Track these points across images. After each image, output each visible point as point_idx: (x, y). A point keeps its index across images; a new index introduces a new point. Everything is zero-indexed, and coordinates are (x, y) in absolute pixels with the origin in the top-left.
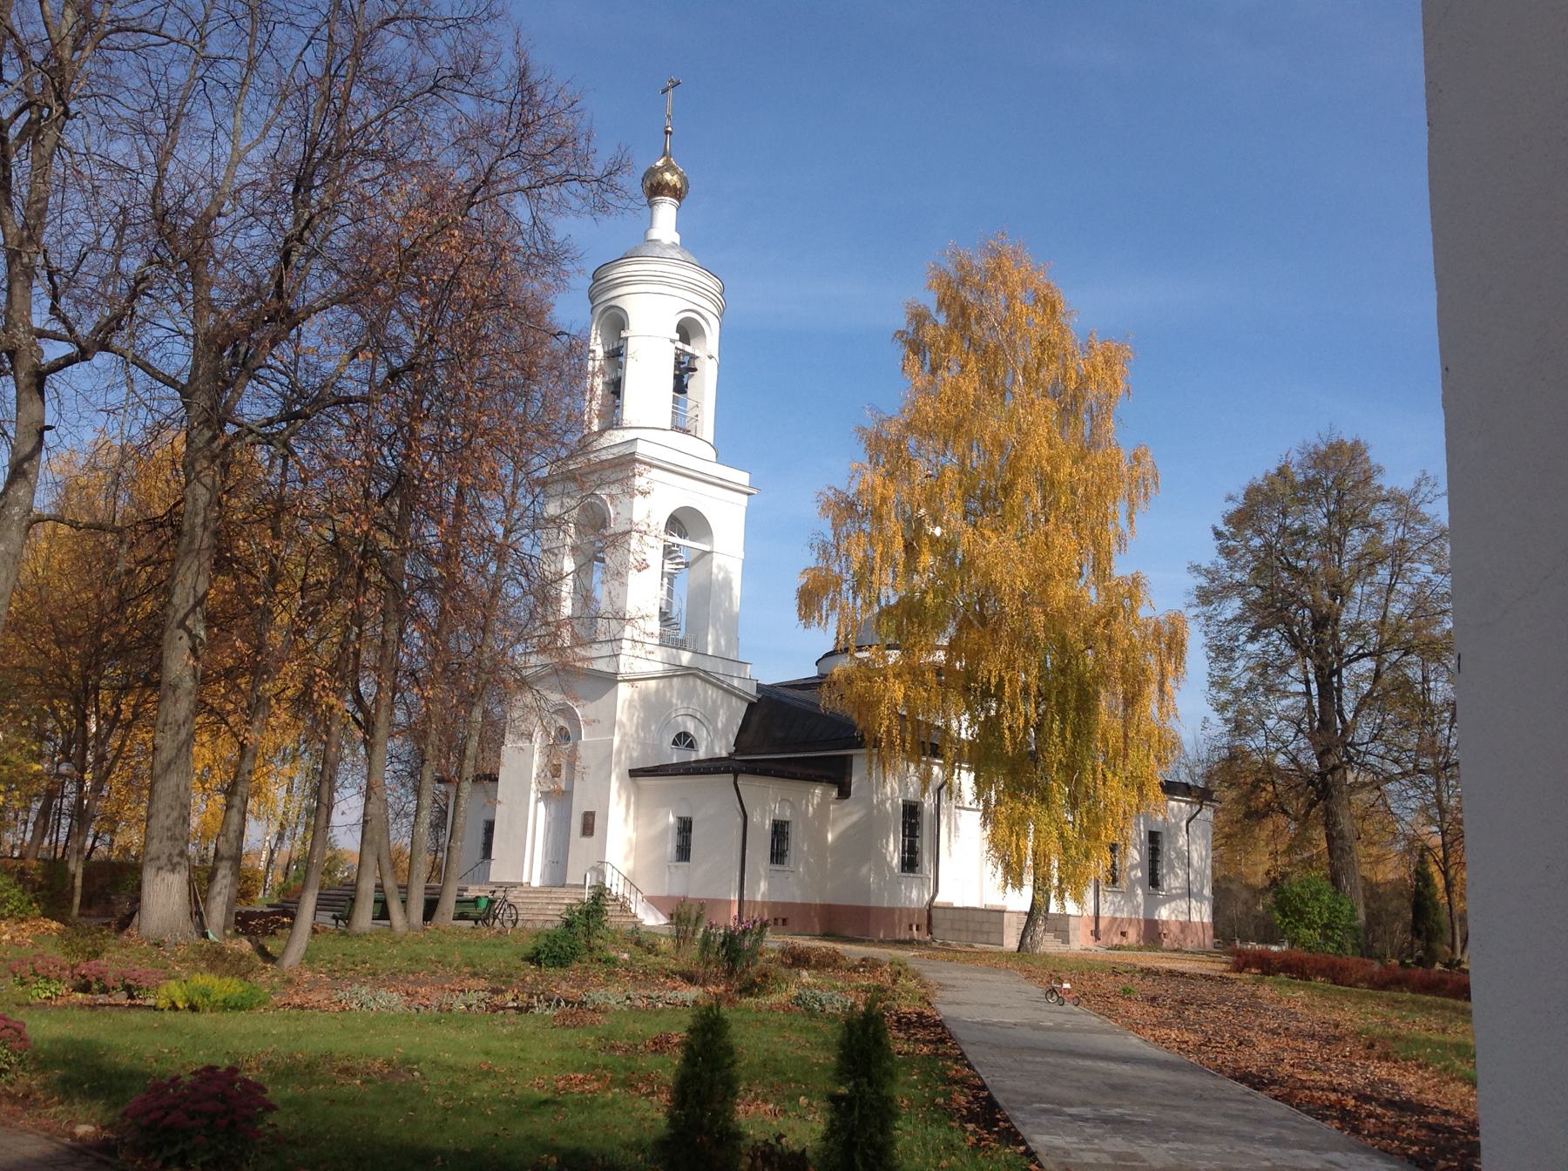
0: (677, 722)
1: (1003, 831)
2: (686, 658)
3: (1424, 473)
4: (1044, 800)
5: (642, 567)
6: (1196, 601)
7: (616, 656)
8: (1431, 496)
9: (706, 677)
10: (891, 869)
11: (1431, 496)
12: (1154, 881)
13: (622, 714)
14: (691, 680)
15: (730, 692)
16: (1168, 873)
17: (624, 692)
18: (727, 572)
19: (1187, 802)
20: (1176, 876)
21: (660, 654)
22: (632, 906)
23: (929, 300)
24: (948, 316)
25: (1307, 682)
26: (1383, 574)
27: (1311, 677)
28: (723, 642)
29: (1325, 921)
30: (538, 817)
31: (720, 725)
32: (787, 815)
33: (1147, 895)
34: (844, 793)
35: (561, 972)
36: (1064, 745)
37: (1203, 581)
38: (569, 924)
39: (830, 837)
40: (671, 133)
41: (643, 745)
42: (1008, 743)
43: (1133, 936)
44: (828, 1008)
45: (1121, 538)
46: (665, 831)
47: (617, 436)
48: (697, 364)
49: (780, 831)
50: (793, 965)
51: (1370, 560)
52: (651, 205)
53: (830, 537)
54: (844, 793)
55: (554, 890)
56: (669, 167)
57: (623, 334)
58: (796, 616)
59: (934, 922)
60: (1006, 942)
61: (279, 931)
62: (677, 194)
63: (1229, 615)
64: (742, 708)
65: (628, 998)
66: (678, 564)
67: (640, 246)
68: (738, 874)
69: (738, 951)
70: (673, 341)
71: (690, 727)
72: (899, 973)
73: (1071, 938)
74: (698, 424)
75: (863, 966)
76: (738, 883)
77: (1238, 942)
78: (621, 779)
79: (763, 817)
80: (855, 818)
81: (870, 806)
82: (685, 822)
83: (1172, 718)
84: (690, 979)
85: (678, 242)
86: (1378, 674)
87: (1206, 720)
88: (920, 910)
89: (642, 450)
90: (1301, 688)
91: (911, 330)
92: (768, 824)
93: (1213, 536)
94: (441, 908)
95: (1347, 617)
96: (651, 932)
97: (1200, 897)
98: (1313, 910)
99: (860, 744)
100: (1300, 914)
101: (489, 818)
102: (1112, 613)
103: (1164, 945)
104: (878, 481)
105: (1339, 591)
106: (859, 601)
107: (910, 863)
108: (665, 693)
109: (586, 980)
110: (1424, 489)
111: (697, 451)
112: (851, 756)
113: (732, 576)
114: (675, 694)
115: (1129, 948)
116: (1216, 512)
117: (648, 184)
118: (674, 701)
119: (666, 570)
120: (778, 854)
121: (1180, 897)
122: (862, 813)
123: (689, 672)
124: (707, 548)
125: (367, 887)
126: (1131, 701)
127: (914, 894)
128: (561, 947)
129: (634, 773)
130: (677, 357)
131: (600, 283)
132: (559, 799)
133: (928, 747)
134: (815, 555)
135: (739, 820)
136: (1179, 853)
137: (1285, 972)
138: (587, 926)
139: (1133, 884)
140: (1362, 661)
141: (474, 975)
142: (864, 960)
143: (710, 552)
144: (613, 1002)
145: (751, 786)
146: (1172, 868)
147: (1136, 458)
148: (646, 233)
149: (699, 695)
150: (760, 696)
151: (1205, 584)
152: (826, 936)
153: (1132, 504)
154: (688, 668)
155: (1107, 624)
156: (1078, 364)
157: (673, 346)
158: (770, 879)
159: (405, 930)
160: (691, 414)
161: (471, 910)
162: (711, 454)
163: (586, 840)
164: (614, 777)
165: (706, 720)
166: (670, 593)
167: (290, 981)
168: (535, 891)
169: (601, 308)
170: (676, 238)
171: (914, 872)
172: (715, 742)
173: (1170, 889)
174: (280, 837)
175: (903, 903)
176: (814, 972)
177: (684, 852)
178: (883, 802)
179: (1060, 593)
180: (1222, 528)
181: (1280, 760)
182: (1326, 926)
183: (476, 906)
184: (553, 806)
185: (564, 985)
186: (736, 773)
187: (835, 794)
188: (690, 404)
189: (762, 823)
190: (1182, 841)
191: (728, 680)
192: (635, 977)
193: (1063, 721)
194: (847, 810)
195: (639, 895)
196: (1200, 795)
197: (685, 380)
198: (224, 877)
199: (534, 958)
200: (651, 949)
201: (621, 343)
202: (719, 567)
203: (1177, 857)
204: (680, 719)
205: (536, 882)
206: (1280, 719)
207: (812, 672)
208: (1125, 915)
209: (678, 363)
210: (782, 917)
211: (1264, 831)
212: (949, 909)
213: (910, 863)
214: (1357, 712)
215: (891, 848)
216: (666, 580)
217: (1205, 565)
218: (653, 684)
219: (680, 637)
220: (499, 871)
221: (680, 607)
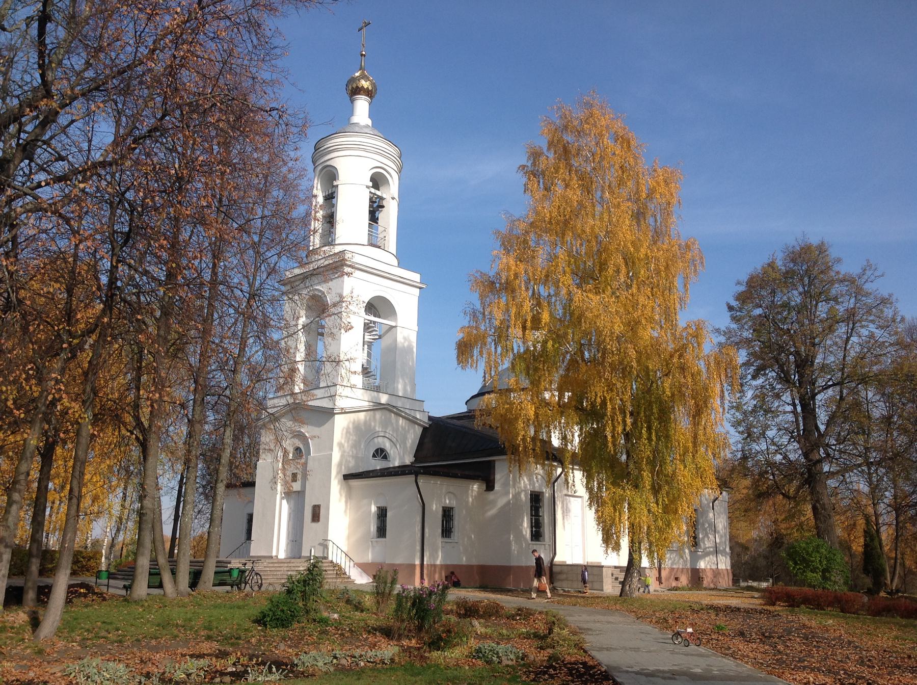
1: (608, 510)
2: (384, 399)
3: (868, 261)
4: (636, 486)
5: (349, 328)
8: (873, 277)
10: (524, 537)
11: (873, 277)
12: (695, 542)
15: (413, 421)
17: (341, 423)
22: (347, 570)
24: (555, 153)
25: (794, 405)
26: (842, 329)
27: (797, 402)
29: (824, 566)
30: (283, 509)
32: (454, 504)
34: (490, 487)
35: (282, 632)
37: (722, 339)
38: (289, 592)
40: (364, 55)
41: (356, 457)
42: (610, 445)
43: (684, 580)
44: (505, 662)
48: (384, 203)
49: (447, 514)
50: (465, 616)
52: (352, 101)
53: (478, 306)
55: (293, 560)
56: (363, 77)
57: (335, 183)
58: (456, 362)
60: (605, 588)
61: (74, 600)
62: (369, 93)
64: (419, 430)
65: (335, 657)
67: (344, 124)
69: (426, 611)
70: (368, 187)
71: (387, 446)
72: (554, 623)
74: (386, 242)
75: (520, 615)
82: (382, 510)
84: (388, 633)
85: (370, 125)
91: (529, 164)
96: (360, 591)
97: (723, 553)
99: (501, 452)
101: (250, 512)
102: (684, 348)
104: (512, 262)
106: (499, 349)
107: (537, 535)
108: (370, 425)
109: (302, 639)
110: (868, 273)
111: (386, 259)
112: (494, 461)
114: (378, 425)
115: (683, 589)
116: (729, 293)
117: (350, 87)
119: (366, 340)
120: (447, 532)
124: (393, 324)
125: (144, 563)
126: (697, 413)
128: (282, 611)
129: (347, 477)
130: (371, 199)
131: (319, 150)
132: (296, 497)
134: (468, 318)
137: (805, 604)
138: (304, 592)
141: (209, 638)
142: (519, 610)
143: (396, 327)
144: (320, 664)
145: (428, 484)
146: (706, 535)
148: (349, 119)
150: (430, 423)
152: (484, 587)
153: (686, 278)
156: (647, 182)
157: (368, 191)
159: (175, 595)
160: (381, 236)
161: (226, 577)
162: (395, 262)
163: (314, 525)
166: (369, 355)
167: (40, 652)
168: (281, 562)
169: (320, 167)
170: (369, 122)
172: (401, 456)
174: (118, 530)
176: (482, 621)
177: (382, 531)
180: (734, 303)
182: (824, 571)
183: (231, 576)
184: (292, 502)
185: (282, 646)
186: (417, 474)
187: (484, 487)
188: (380, 229)
189: (435, 508)
191: (412, 413)
193: (649, 429)
195: (352, 562)
197: (376, 215)
199: (261, 621)
200: (359, 607)
201: (334, 189)
205: (282, 555)
206: (779, 430)
207: (464, 409)
209: (372, 201)
210: (454, 578)
211: (768, 505)
212: (563, 565)
213: (537, 535)
214: (828, 424)
216: (366, 346)
218: (362, 416)
219: (376, 384)
220: (256, 550)
221: (375, 366)
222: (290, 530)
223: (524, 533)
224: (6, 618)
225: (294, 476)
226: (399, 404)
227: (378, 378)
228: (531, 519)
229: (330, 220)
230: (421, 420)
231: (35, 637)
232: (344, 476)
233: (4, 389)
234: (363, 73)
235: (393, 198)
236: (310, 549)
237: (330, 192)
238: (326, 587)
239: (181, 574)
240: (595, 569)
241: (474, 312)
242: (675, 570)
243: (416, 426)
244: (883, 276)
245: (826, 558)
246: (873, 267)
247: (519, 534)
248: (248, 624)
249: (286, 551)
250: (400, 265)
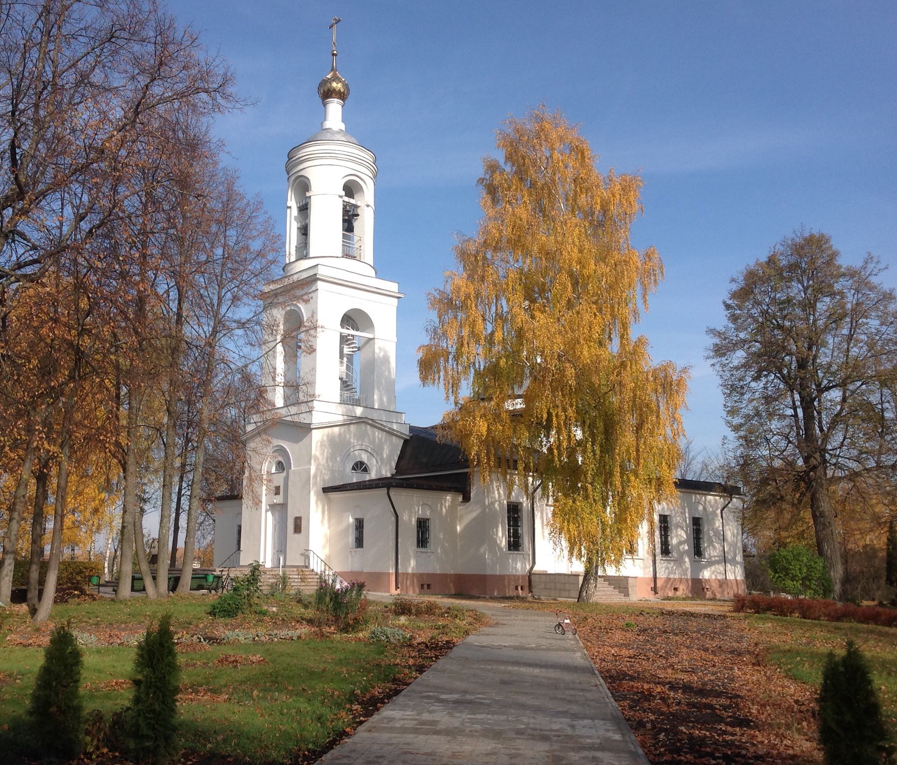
0: (355, 454)
2: (359, 411)
6: (712, 354)
7: (310, 412)
8: (876, 271)
9: (373, 424)
10: (500, 549)
11: (876, 271)
12: (698, 551)
13: (316, 451)
14: (363, 426)
15: (391, 433)
16: (709, 546)
17: (317, 436)
18: (385, 352)
19: (721, 497)
20: (715, 548)
21: (341, 409)
23: (500, 157)
25: (795, 409)
27: (798, 403)
28: (385, 399)
29: (804, 575)
30: (268, 521)
31: (385, 456)
32: (428, 514)
33: (692, 562)
34: (466, 498)
35: (228, 620)
36: (595, 459)
39: (458, 528)
40: (336, 55)
41: (332, 471)
45: (635, 312)
46: (348, 527)
47: (304, 264)
48: (359, 211)
49: (423, 526)
51: (836, 318)
52: (325, 105)
54: (466, 498)
56: (336, 78)
57: (308, 194)
59: (533, 584)
62: (342, 96)
63: (736, 363)
65: (257, 636)
66: (353, 348)
67: (318, 133)
68: (394, 555)
70: (341, 197)
71: (364, 457)
73: (630, 592)
74: (362, 252)
75: (448, 613)
76: (394, 562)
77: (772, 593)
78: (317, 494)
79: (410, 517)
80: (474, 515)
81: (483, 506)
83: (682, 437)
85: (344, 129)
86: (844, 400)
87: (725, 438)
88: (523, 576)
89: (322, 271)
90: (790, 412)
91: (488, 177)
92: (414, 521)
93: (724, 308)
94: (181, 583)
95: (823, 360)
97: (734, 562)
98: (795, 568)
100: (786, 570)
101: (239, 524)
103: (707, 596)
105: (814, 341)
107: (515, 544)
108: (345, 437)
110: (871, 266)
112: (467, 473)
113: (389, 354)
114: (352, 436)
115: (677, 599)
116: (724, 290)
117: (322, 92)
118: (352, 440)
120: (422, 541)
121: (718, 562)
122: (479, 511)
123: (361, 421)
124: (371, 336)
127: (519, 566)
128: (229, 604)
129: (326, 490)
132: (280, 509)
133: (511, 463)
135: (393, 519)
136: (716, 533)
139: (681, 554)
140: (831, 391)
142: (449, 608)
143: (373, 339)
146: (711, 543)
147: (648, 256)
149: (369, 437)
150: (411, 435)
151: (719, 342)
154: (360, 418)
155: (619, 374)
158: (417, 558)
160: (356, 246)
162: (372, 272)
163: (296, 535)
164: (312, 493)
165: (375, 452)
169: (293, 178)
170: (342, 126)
171: (518, 550)
173: (711, 557)
175: (511, 571)
177: (359, 542)
178: (493, 503)
179: (586, 354)
181: (777, 463)
182: (803, 579)
184: (277, 514)
187: (461, 499)
188: (356, 239)
189: (409, 520)
190: (718, 523)
192: (275, 623)
194: (470, 509)
196: (729, 491)
198: (10, 565)
201: (307, 200)
202: (380, 349)
203: (715, 535)
204: (357, 452)
208: (677, 576)
209: (345, 212)
213: (515, 544)
215: (500, 534)
216: (345, 359)
217: (720, 328)
218: (336, 429)
219: (356, 397)
222: (276, 541)
223: (498, 542)
224: (13, 608)
225: (277, 489)
226: (375, 416)
227: (358, 390)
228: (509, 530)
229: (304, 231)
230: (397, 431)
231: (34, 621)
232: (323, 489)
233: (2, 439)
234: (335, 74)
235: (368, 206)
236: (294, 559)
237: (304, 203)
239: (160, 578)
240: (544, 576)
241: (435, 329)
242: (672, 581)
243: (394, 437)
244: (886, 268)
245: (806, 566)
246: (875, 260)
247: (494, 543)
248: (204, 614)
249: (272, 561)
250: (378, 275)
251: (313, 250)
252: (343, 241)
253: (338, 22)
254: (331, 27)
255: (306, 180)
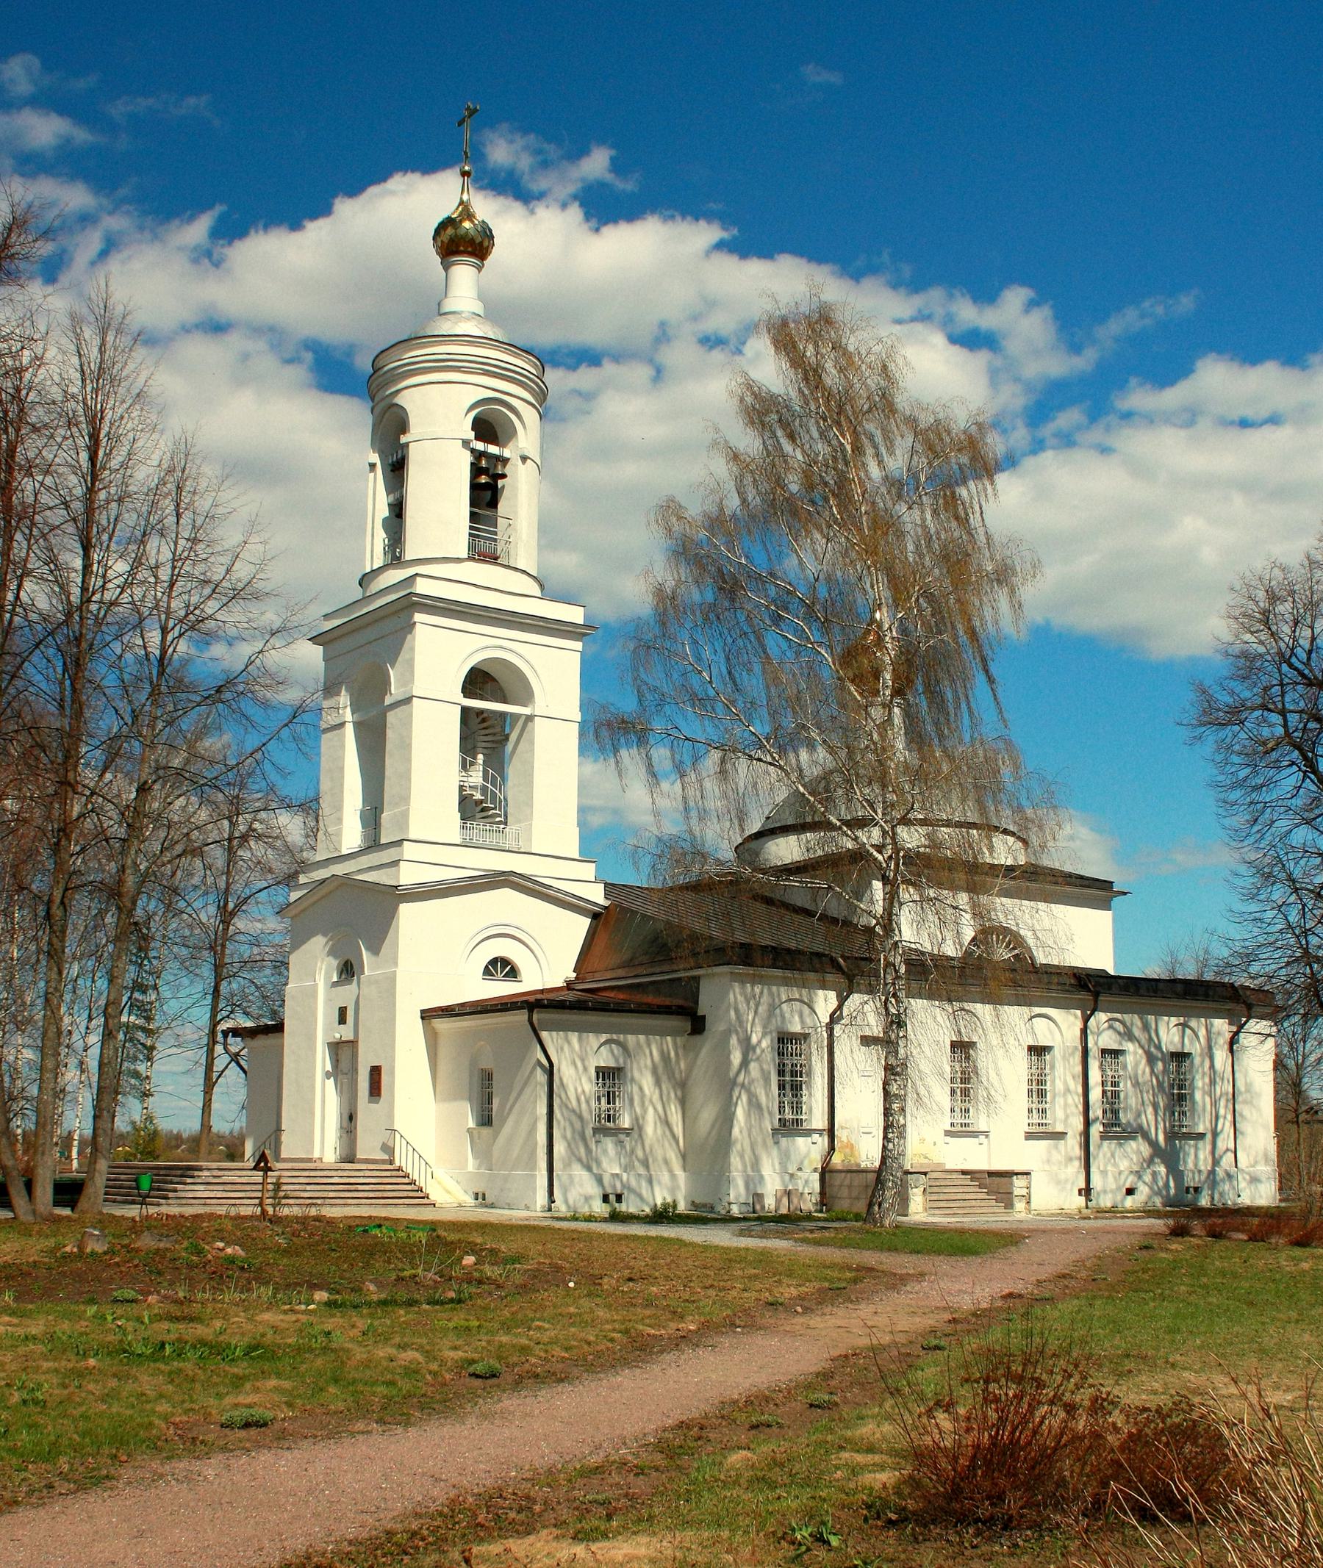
57: (403, 439)
143: (530, 718)
150: (607, 903)
169: (382, 405)
209: (476, 470)
235: (524, 459)
237: (400, 456)
238: (881, 1035)
251: (412, 550)
252: (471, 528)
253: (472, 112)
254: (461, 123)
255: (404, 415)
